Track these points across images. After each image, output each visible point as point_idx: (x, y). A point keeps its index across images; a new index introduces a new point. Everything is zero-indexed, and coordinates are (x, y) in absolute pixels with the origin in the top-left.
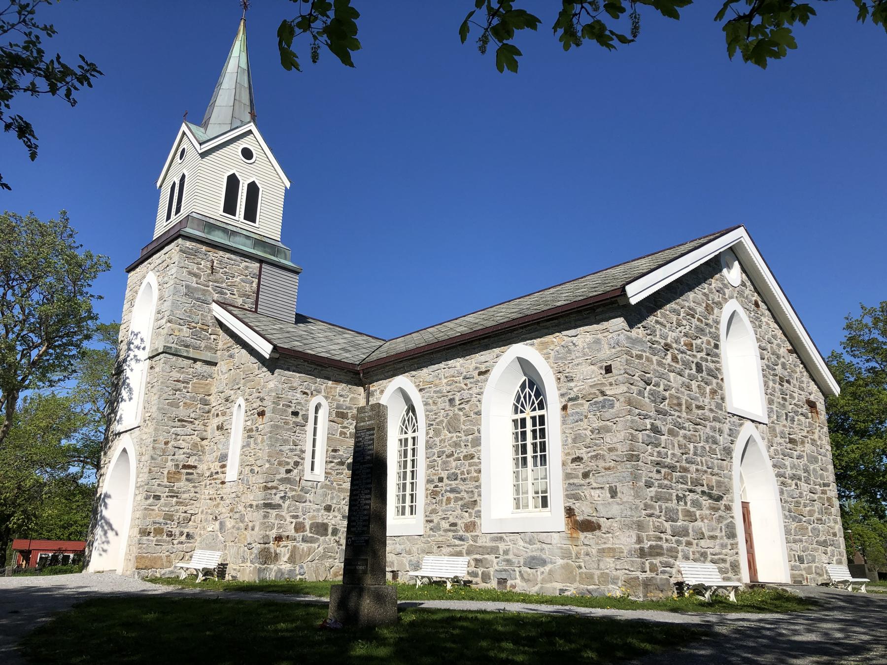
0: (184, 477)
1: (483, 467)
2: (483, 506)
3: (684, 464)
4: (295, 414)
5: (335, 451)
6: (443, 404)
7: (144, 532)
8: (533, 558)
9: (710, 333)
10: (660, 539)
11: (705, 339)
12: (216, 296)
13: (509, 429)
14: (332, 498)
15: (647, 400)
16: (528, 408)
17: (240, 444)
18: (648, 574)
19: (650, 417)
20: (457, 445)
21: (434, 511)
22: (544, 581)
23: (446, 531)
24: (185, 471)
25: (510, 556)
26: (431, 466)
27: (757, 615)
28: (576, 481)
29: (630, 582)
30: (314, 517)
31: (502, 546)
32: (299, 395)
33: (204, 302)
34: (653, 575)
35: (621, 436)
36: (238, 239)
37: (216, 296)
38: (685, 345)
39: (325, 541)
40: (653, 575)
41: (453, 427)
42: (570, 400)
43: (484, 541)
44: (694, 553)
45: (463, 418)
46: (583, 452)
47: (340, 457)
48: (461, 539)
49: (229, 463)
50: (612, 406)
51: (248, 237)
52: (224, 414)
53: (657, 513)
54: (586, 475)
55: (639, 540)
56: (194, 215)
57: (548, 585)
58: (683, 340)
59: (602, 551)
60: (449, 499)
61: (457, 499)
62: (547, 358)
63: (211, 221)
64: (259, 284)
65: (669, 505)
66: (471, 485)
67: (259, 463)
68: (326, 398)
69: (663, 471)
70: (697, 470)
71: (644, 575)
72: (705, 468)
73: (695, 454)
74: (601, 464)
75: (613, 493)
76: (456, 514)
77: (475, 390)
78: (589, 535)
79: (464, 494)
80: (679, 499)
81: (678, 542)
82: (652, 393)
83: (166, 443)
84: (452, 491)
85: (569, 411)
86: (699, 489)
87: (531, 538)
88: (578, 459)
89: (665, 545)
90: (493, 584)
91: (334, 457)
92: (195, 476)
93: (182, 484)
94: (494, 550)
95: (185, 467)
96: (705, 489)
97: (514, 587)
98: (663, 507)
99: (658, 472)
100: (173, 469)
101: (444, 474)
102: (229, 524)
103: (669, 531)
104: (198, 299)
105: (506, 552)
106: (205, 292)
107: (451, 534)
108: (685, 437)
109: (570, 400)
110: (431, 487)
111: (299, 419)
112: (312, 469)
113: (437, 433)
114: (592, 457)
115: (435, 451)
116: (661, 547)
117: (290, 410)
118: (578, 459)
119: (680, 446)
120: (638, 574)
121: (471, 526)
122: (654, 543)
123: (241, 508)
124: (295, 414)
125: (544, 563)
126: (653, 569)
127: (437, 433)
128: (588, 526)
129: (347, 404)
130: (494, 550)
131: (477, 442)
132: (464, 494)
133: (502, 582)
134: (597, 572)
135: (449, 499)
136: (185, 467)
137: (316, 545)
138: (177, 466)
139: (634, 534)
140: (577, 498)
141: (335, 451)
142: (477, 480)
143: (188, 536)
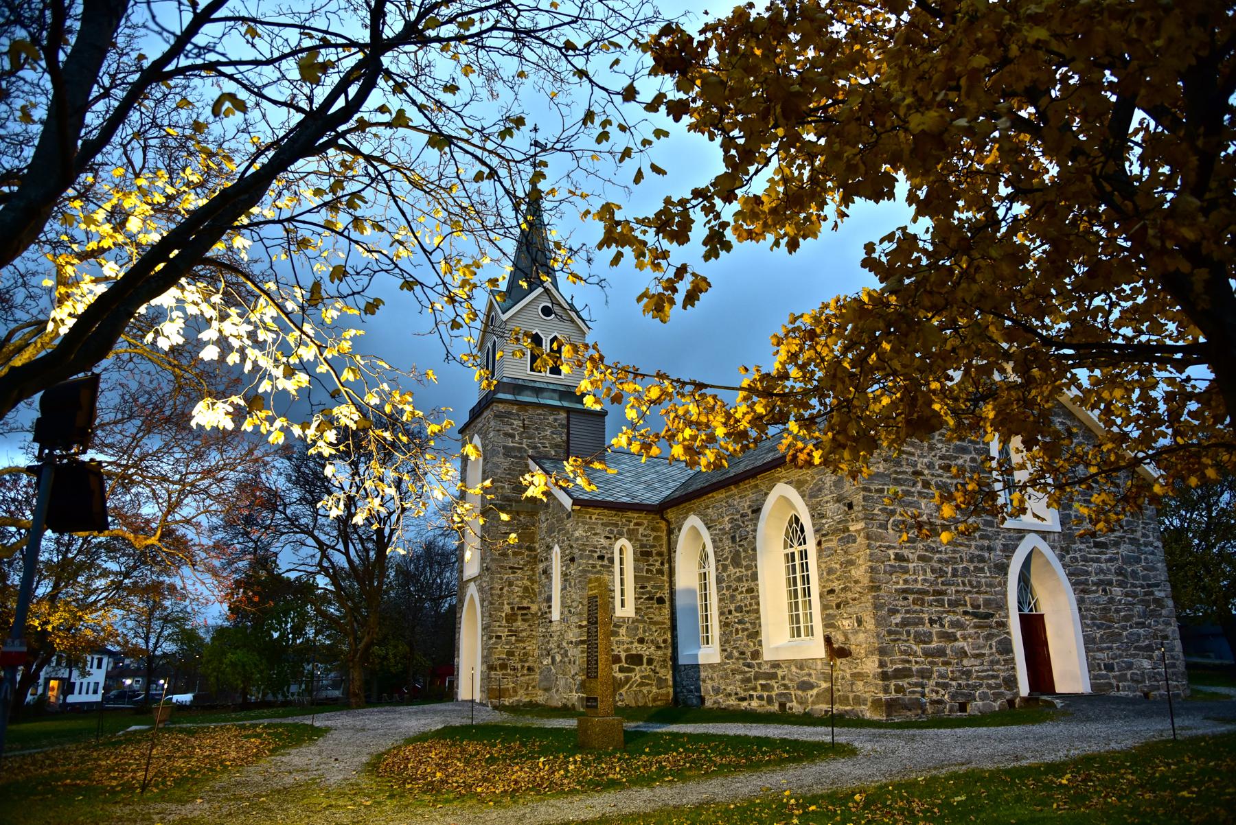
0: (520, 618)
1: (761, 599)
2: (764, 637)
3: (940, 587)
4: (601, 558)
5: (642, 587)
6: (727, 542)
7: (491, 668)
8: (804, 682)
9: (975, 449)
10: (909, 662)
11: (968, 457)
12: (530, 452)
13: (782, 564)
14: (644, 631)
15: (890, 531)
16: (796, 544)
17: (559, 587)
18: (894, 695)
19: (894, 548)
20: (740, 579)
21: (727, 641)
22: (813, 703)
23: (737, 659)
24: (520, 612)
25: (787, 682)
26: (721, 600)
27: (770, 735)
28: (831, 612)
29: (877, 703)
30: (627, 650)
31: (780, 673)
32: (603, 541)
33: (521, 458)
34: (900, 696)
35: (863, 569)
36: (546, 394)
37: (530, 452)
38: (941, 467)
39: (641, 671)
40: (900, 696)
41: (736, 563)
42: (824, 535)
43: (766, 668)
44: (952, 672)
45: (743, 555)
46: (836, 585)
47: (649, 592)
48: (749, 666)
49: (553, 604)
50: (854, 541)
51: (554, 391)
52: (546, 559)
53: (905, 637)
54: (838, 606)
55: (882, 664)
56: (505, 380)
57: (816, 707)
58: (938, 463)
59: (853, 675)
60: (737, 630)
61: (744, 630)
62: (803, 497)
63: (520, 382)
64: (568, 434)
65: (920, 628)
66: (753, 616)
67: (574, 604)
68: (630, 540)
69: (911, 598)
70: (957, 592)
71: (888, 697)
72: (968, 588)
73: (954, 575)
74: (850, 595)
75: (860, 622)
76: (742, 640)
77: (750, 528)
78: (844, 660)
79: (748, 625)
80: (932, 622)
81: (933, 663)
82: (896, 524)
83: (501, 589)
84: (740, 622)
85: (824, 545)
86: (961, 609)
87: (801, 664)
88: (832, 591)
89: (915, 667)
90: (775, 707)
91: (643, 593)
92: (529, 617)
93: (519, 624)
94: (773, 676)
95: (519, 608)
96: (969, 609)
97: (791, 708)
98: (912, 631)
99: (905, 599)
100: (509, 611)
101: (732, 607)
102: (558, 658)
103: (919, 652)
104: (515, 457)
105: (783, 678)
106: (519, 450)
107: (741, 662)
108: (940, 561)
109: (824, 535)
110: (724, 620)
111: (606, 562)
112: (623, 606)
113: (725, 568)
114: (842, 589)
115: (724, 585)
116: (910, 669)
117: (596, 555)
118: (832, 591)
119: (933, 571)
120: (881, 695)
121: (756, 654)
122: (900, 666)
123: (564, 644)
124: (601, 558)
125: (811, 687)
126: (899, 689)
127: (725, 568)
128: (843, 653)
129: (651, 542)
130: (773, 676)
131: (755, 577)
132: (748, 625)
133: (782, 705)
134: (851, 695)
135: (737, 630)
136: (519, 608)
137: (632, 674)
138: (512, 609)
139: (876, 658)
140: (832, 626)
141: (642, 587)
142: (757, 611)
143: (529, 669)
